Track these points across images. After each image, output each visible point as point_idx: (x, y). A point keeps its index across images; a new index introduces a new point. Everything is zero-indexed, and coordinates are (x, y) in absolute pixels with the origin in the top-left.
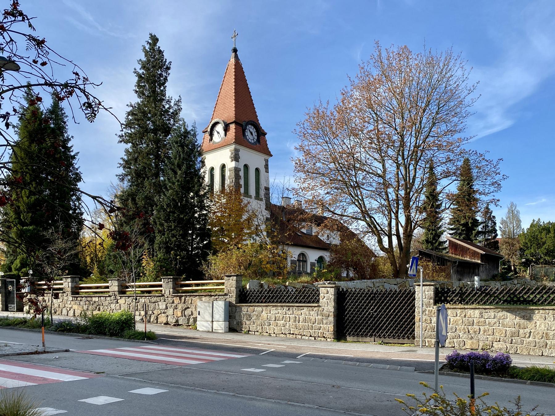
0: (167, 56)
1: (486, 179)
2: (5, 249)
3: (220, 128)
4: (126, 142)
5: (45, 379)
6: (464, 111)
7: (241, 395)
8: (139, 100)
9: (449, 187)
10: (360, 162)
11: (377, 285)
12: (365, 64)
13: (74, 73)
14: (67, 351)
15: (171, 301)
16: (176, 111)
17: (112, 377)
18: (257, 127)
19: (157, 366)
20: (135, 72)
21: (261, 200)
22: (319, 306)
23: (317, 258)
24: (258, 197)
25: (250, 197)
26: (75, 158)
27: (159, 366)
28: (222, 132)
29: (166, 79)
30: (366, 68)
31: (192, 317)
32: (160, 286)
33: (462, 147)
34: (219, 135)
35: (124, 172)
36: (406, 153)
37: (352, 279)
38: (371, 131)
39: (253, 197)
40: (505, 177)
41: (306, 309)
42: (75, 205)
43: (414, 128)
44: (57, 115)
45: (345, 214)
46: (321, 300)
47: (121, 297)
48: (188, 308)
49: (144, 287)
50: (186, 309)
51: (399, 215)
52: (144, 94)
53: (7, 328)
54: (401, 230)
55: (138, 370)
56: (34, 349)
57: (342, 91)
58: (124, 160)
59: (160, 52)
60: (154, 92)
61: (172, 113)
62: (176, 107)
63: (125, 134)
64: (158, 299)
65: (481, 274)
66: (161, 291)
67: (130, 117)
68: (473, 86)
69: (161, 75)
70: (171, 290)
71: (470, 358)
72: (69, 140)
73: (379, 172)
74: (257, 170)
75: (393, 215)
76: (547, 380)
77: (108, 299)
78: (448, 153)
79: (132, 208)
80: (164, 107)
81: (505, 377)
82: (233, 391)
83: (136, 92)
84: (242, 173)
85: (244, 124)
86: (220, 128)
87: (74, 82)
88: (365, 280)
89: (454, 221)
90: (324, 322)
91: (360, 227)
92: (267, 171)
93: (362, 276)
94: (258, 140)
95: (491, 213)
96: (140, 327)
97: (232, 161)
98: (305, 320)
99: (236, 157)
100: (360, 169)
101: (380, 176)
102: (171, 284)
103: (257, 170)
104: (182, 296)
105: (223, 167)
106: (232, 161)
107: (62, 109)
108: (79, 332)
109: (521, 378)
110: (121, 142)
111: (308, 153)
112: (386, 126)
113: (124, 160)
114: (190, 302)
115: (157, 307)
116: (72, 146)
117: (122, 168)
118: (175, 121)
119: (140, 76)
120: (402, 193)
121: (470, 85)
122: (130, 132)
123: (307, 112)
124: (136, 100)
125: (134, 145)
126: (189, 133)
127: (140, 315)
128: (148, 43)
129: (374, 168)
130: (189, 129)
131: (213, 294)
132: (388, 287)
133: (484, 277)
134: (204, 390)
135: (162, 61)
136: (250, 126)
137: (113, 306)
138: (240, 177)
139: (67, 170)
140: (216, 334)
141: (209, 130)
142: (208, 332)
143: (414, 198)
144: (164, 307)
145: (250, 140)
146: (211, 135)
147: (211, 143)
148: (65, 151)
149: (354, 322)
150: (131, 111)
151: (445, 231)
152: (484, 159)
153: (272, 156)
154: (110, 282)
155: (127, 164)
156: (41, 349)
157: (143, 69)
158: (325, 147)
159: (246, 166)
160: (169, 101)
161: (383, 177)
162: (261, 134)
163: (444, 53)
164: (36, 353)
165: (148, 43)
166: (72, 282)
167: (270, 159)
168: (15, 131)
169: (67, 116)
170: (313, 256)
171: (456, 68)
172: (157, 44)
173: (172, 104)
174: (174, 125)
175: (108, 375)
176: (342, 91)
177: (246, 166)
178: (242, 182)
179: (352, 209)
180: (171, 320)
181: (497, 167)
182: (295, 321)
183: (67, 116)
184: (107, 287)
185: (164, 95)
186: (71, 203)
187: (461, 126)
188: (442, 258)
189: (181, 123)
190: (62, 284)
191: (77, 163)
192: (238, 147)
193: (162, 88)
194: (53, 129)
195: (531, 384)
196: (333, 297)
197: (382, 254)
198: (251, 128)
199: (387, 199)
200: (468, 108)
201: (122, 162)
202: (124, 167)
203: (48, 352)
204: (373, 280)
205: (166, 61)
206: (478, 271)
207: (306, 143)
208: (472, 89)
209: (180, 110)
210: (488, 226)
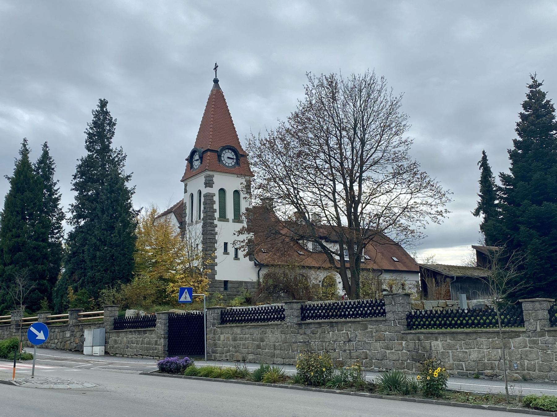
25: (227, 220)
32: (67, 317)
44: (46, 164)
66: (67, 321)
94: (237, 163)
105: (200, 192)
124: (85, 153)
138: (215, 202)
190: (9, 318)
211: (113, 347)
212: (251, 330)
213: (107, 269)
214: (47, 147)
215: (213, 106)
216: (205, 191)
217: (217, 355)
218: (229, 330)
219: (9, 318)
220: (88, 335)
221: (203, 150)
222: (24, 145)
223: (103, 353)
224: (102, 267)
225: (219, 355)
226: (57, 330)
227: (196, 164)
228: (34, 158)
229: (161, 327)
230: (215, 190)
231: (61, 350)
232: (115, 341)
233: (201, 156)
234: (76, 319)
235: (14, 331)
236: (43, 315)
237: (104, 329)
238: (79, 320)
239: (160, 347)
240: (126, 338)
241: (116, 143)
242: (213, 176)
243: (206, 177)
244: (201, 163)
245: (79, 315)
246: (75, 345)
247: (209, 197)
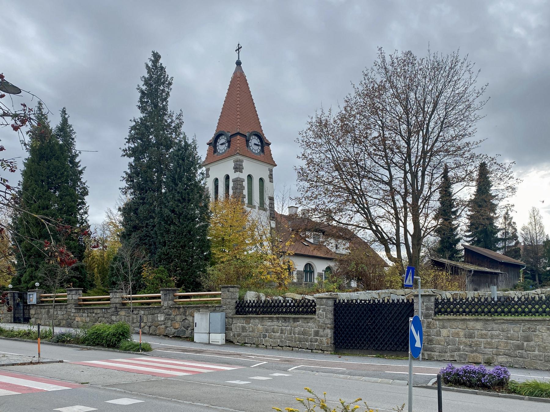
0: (169, 72)
1: (499, 184)
2: (16, 262)
4: (129, 156)
5: (30, 389)
6: (472, 114)
7: (215, 407)
8: (142, 115)
9: (464, 192)
10: (363, 168)
11: (383, 296)
12: (369, 71)
13: (22, 104)
14: (61, 362)
16: (178, 124)
17: (95, 387)
18: (260, 137)
19: (142, 378)
20: (138, 89)
21: (265, 210)
23: (324, 268)
24: (262, 206)
25: (254, 207)
26: (82, 173)
27: (146, 377)
29: (168, 94)
30: (369, 75)
32: (159, 297)
33: (473, 151)
35: (127, 186)
36: (413, 159)
37: (356, 290)
38: (375, 138)
40: (519, 181)
42: (82, 219)
43: (421, 133)
44: (65, 133)
45: (351, 223)
49: (137, 300)
51: (408, 223)
52: (146, 110)
53: (11, 340)
54: (410, 238)
55: (123, 381)
56: (29, 360)
57: (346, 99)
58: (127, 173)
59: (162, 68)
60: (156, 106)
61: (174, 127)
62: (178, 121)
63: (129, 148)
65: (500, 284)
66: (160, 303)
67: (133, 132)
68: (482, 89)
69: (163, 91)
71: (465, 372)
72: (77, 155)
73: (385, 179)
74: (261, 180)
75: (401, 224)
76: (544, 394)
78: (455, 158)
79: (136, 219)
80: (166, 121)
81: (502, 392)
82: (208, 403)
83: (139, 107)
85: (247, 134)
87: (23, 113)
88: (370, 291)
89: (472, 227)
91: (367, 236)
92: (271, 181)
93: (368, 287)
94: (262, 150)
95: (512, 218)
96: (136, 339)
100: (364, 177)
101: (386, 183)
105: (227, 177)
107: (71, 126)
108: (78, 343)
109: (519, 393)
110: (124, 156)
111: (311, 162)
112: (391, 132)
113: (127, 173)
116: (80, 162)
117: (124, 182)
118: (176, 135)
119: (142, 92)
120: (409, 200)
121: (478, 88)
122: (133, 146)
123: (310, 121)
124: (139, 115)
125: (137, 160)
126: (190, 145)
128: (151, 60)
129: (380, 176)
130: (190, 142)
131: (210, 306)
132: (394, 297)
133: (504, 287)
134: (180, 401)
135: (164, 76)
136: (254, 137)
138: (244, 187)
139: (74, 186)
140: (212, 347)
142: (206, 344)
143: (422, 206)
145: (254, 151)
148: (73, 166)
150: (134, 126)
151: (462, 238)
152: (495, 163)
155: (130, 178)
156: (36, 360)
157: (146, 85)
158: (328, 156)
159: (250, 177)
160: (171, 116)
161: (389, 183)
162: (264, 144)
163: (450, 57)
164: (31, 363)
165: (151, 60)
167: (274, 169)
168: (27, 149)
169: (75, 133)
170: (320, 267)
171: (463, 72)
172: (160, 61)
173: (174, 118)
174: (176, 138)
175: (92, 386)
176: (346, 99)
177: (250, 177)
179: (359, 218)
181: (510, 171)
183: (75, 133)
184: (108, 299)
185: (166, 110)
186: (78, 217)
187: (470, 130)
188: (455, 267)
189: (182, 136)
190: (66, 296)
191: (84, 178)
193: (164, 103)
194: (61, 145)
195: (530, 400)
197: (391, 263)
199: (395, 208)
200: (476, 112)
201: (125, 176)
202: (127, 181)
203: (43, 363)
204: (378, 291)
205: (168, 77)
206: (497, 280)
207: (309, 151)
208: (481, 92)
209: (182, 123)
210: (508, 232)
211: (239, 335)
212: (505, 326)
213: (185, 246)
214: (66, 114)
215: (238, 89)
216: (233, 176)
217: (433, 353)
218: (460, 325)
219: (66, 296)
220: (201, 320)
221: (230, 134)
222: (40, 109)
223: (224, 343)
224: (179, 242)
225: (437, 354)
226: (142, 312)
227: (221, 148)
228: (54, 123)
229: (325, 316)
230: (244, 176)
231: (151, 334)
232: (244, 329)
233: (229, 140)
234: (172, 300)
235: (73, 311)
236: (118, 295)
237: (224, 314)
238: (175, 302)
239: (324, 339)
240: (257, 325)
241: (173, 105)
242: (242, 161)
243: (236, 161)
244: (229, 146)
245: (175, 296)
246: (173, 330)
247: (238, 181)
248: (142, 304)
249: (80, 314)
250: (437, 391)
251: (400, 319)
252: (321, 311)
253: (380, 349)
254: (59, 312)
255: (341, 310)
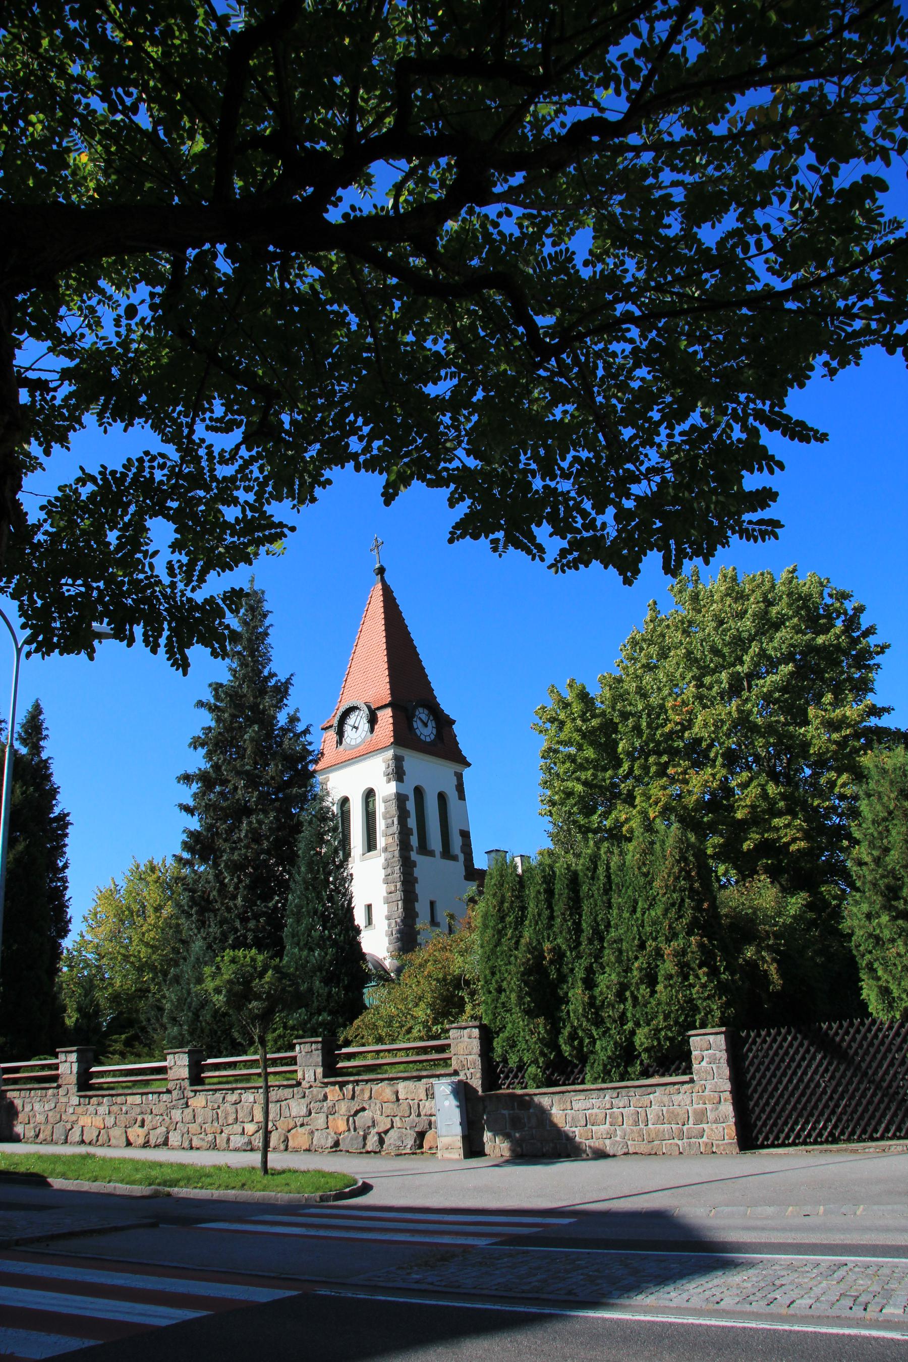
3: (359, 719)
15: (321, 1097)
21: (455, 858)
22: (692, 1081)
28: (364, 726)
31: (373, 1131)
34: (357, 731)
39: (438, 854)
41: (659, 1090)
46: (695, 1066)
47: (195, 1091)
48: (363, 1109)
50: (357, 1113)
64: (288, 1092)
70: (320, 1070)
74: (442, 797)
77: (165, 1097)
84: (411, 805)
86: (359, 719)
90: (711, 1116)
92: (462, 797)
97: (389, 781)
98: (661, 1120)
99: (398, 773)
102: (318, 1057)
103: (442, 797)
104: (348, 1082)
105: (370, 794)
106: (389, 781)
114: (367, 1095)
115: (286, 1112)
127: (243, 1133)
136: (421, 710)
137: (177, 1114)
141: (335, 722)
144: (304, 1111)
145: (422, 737)
146: (340, 733)
147: (341, 748)
149: (786, 1053)
153: (469, 765)
154: (169, 1057)
159: (418, 791)
162: (444, 723)
166: (79, 1061)
167: (467, 773)
177: (418, 791)
178: (412, 823)
180: (323, 1142)
182: (636, 1123)
184: (163, 1070)
192: (403, 752)
196: (724, 1055)
198: (422, 713)
248: (113, 1089)
249: (91, 1108)
250: (270, 1165)
251: (762, 1063)
252: (704, 1064)
253: (845, 1137)
254: (37, 1107)
255: (296, 1064)
